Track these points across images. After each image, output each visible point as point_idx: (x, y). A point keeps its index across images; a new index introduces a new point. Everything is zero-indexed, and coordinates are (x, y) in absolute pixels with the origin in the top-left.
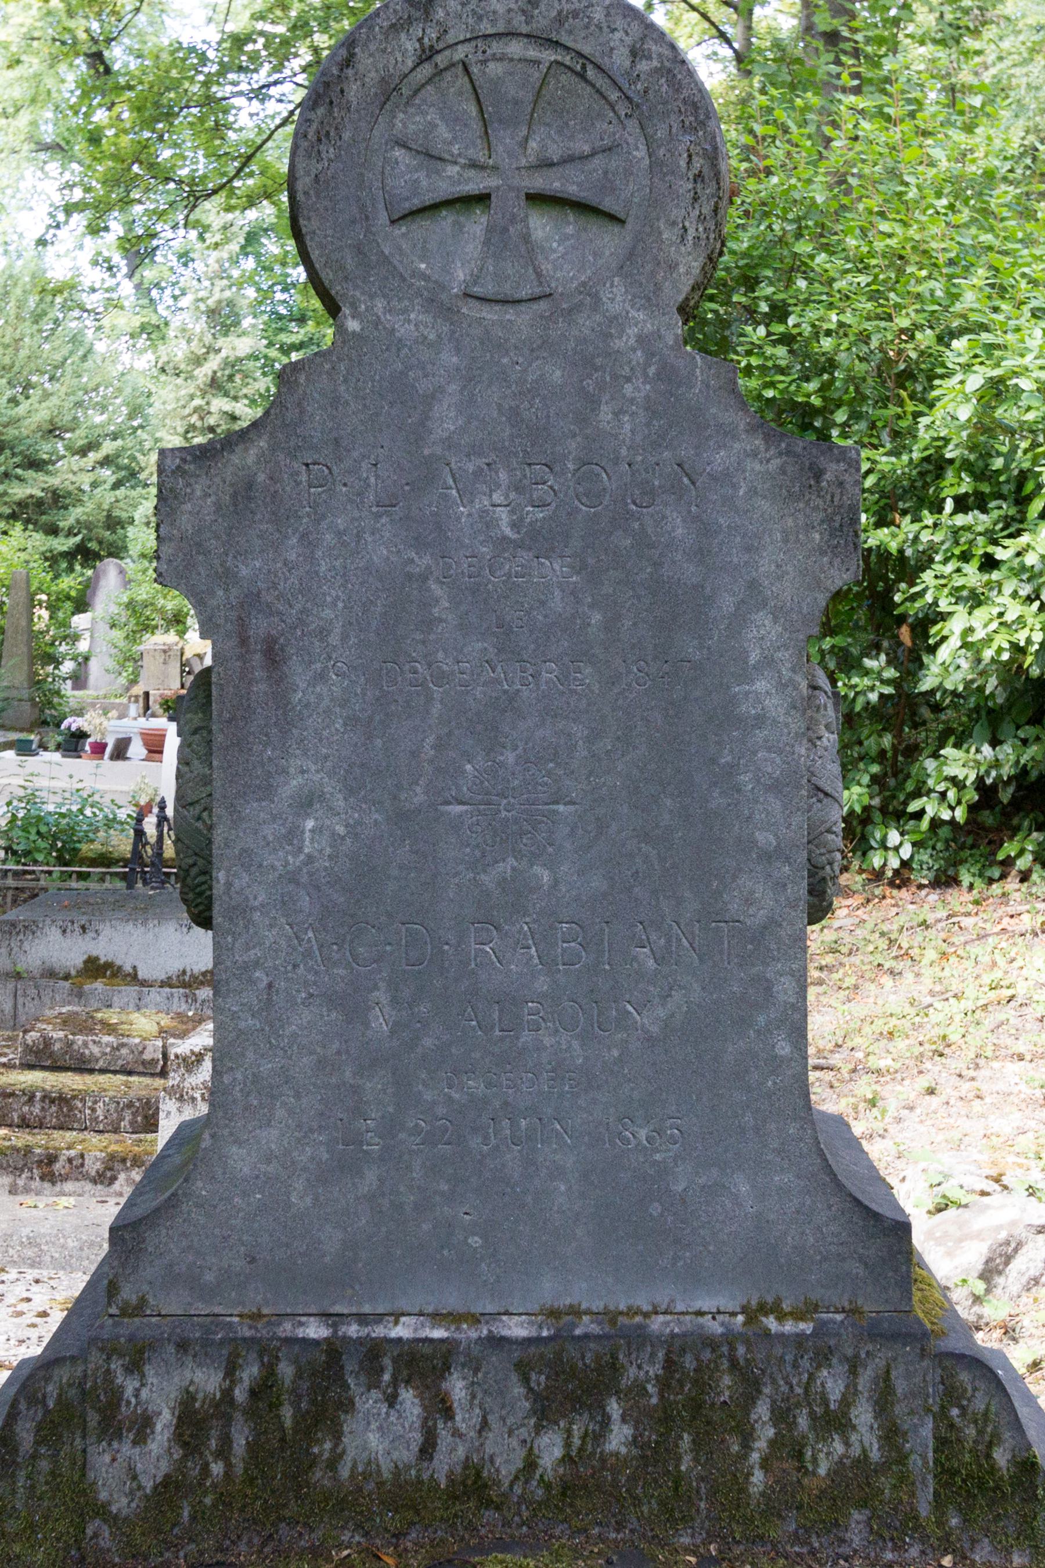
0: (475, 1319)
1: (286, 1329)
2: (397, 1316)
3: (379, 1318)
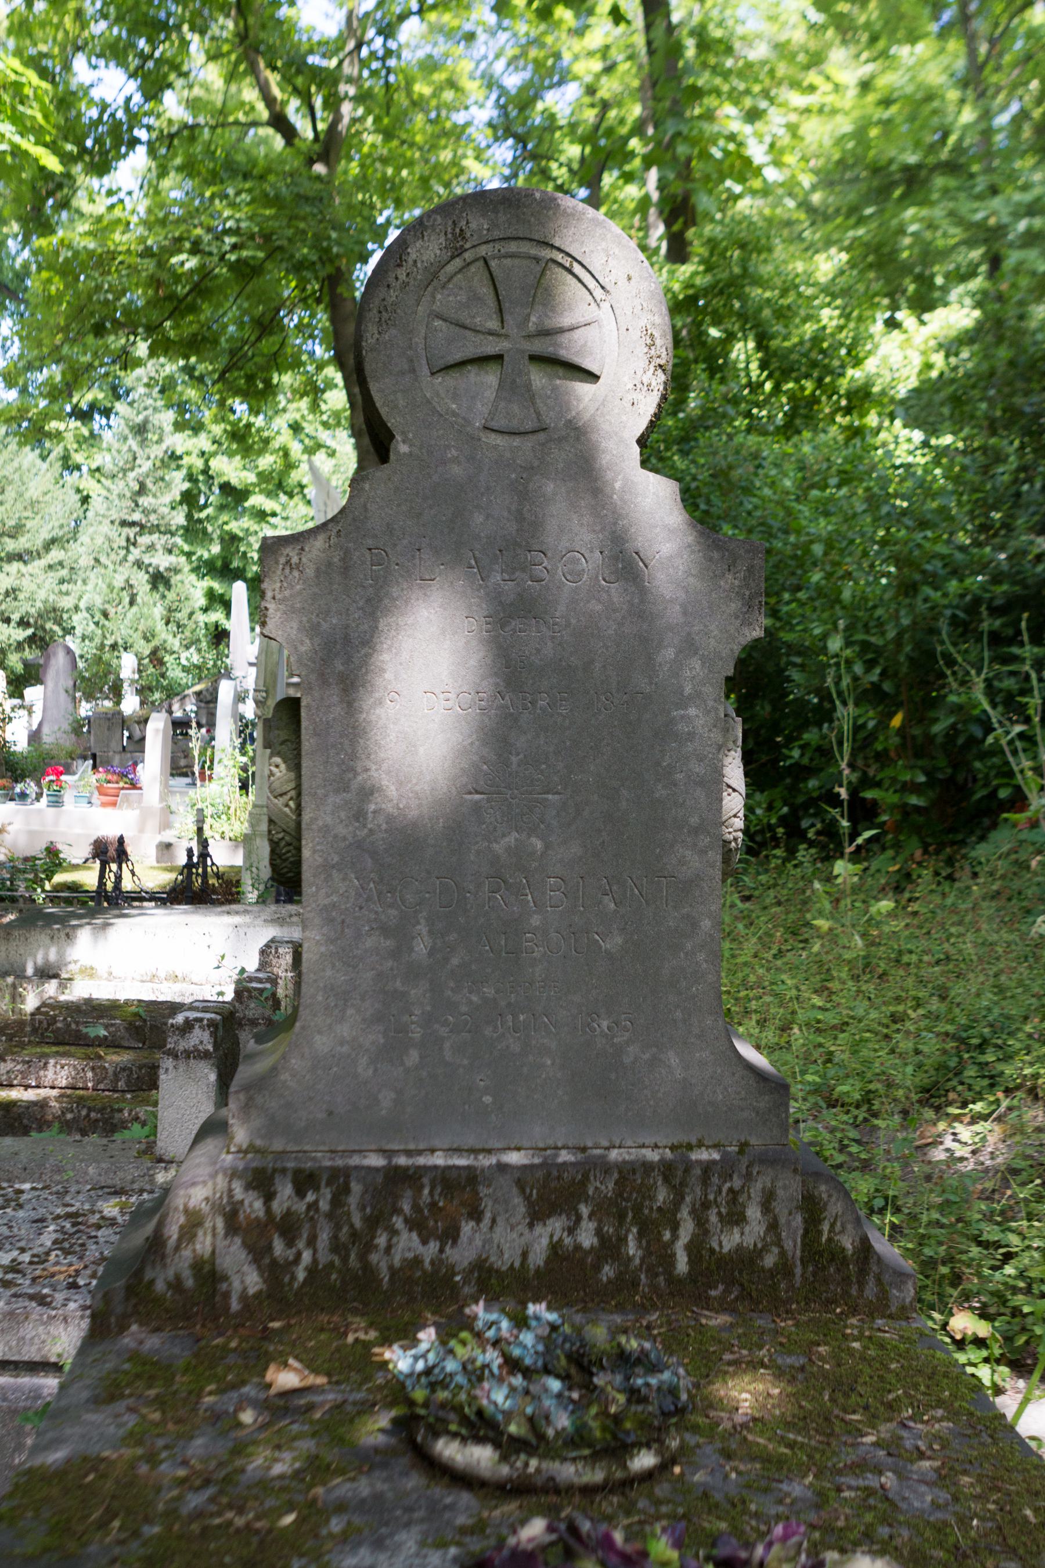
0: (489, 1151)
1: (355, 1161)
2: (433, 1151)
3: (420, 1152)
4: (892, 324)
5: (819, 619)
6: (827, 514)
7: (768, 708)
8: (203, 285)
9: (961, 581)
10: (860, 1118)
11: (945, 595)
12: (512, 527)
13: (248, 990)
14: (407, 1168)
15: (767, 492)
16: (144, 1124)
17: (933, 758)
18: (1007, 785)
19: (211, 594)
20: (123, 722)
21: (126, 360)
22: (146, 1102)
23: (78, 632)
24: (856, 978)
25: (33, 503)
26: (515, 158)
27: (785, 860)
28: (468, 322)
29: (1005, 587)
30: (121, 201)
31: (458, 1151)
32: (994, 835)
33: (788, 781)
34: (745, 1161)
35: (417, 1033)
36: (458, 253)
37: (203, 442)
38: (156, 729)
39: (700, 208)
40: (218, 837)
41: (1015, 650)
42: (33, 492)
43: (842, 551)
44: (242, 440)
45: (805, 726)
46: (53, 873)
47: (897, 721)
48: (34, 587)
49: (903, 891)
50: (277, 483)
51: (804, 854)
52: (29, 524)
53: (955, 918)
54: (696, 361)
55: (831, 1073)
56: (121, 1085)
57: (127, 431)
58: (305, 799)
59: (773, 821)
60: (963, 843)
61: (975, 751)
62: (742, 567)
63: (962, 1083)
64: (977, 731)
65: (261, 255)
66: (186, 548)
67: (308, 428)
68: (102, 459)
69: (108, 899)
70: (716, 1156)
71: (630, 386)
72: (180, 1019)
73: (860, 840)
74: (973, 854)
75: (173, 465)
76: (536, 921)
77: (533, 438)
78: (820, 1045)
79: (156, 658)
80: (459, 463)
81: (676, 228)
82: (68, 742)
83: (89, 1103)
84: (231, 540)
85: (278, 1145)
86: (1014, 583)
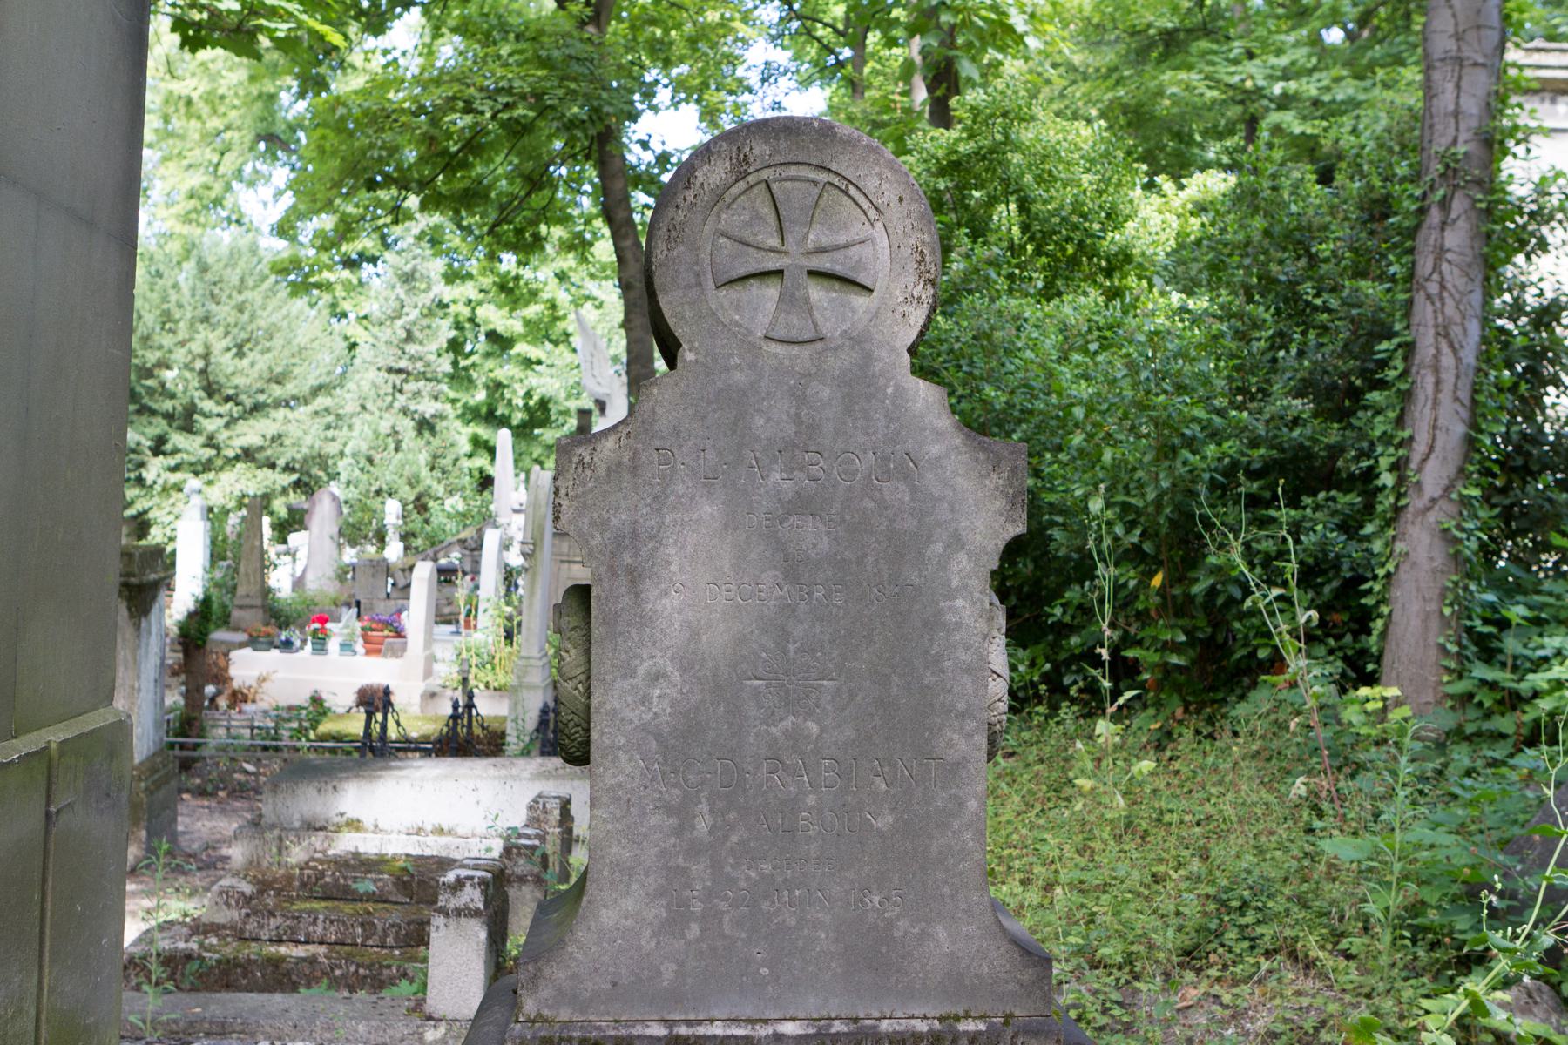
0: (766, 1021)
1: (638, 1030)
2: (712, 1021)
3: (699, 1022)
4: (1150, 186)
5: (1080, 480)
6: (1087, 378)
7: (1031, 566)
8: (474, 145)
9: (1219, 445)
10: (1122, 981)
11: (1204, 458)
12: (791, 430)
13: (518, 847)
14: (688, 1038)
15: (1029, 354)
16: (412, 981)
17: (1193, 617)
18: (1266, 645)
19: (477, 442)
20: (388, 570)
21: (398, 214)
22: (414, 959)
23: (343, 478)
24: (1118, 839)
25: (301, 350)
26: (781, 18)
27: (1048, 717)
28: (750, 239)
29: (1262, 451)
30: (395, 60)
31: (736, 1021)
32: (1253, 695)
33: (1050, 637)
34: (1010, 1032)
35: (697, 908)
36: (742, 176)
37: (469, 290)
38: (423, 572)
39: (963, 74)
40: (482, 687)
41: (1273, 513)
42: (302, 339)
43: (1103, 413)
44: (510, 292)
45: (1067, 583)
46: (318, 722)
47: (1157, 581)
48: (300, 433)
49: (1164, 749)
50: (542, 331)
51: (1066, 711)
52: (296, 371)
53: (1215, 778)
54: (959, 225)
55: (1094, 935)
56: (390, 941)
57: (395, 280)
58: (594, 683)
59: (1036, 679)
60: (1224, 701)
61: (1234, 611)
62: (1006, 468)
63: (1222, 945)
64: (1238, 594)
65: (532, 114)
66: (452, 394)
67: (575, 278)
68: (372, 307)
69: (372, 749)
70: (982, 1027)
71: (901, 299)
72: (451, 877)
73: (1121, 701)
74: (1233, 713)
75: (441, 313)
76: (811, 800)
77: (812, 346)
78: (1083, 906)
79: (421, 505)
80: (742, 370)
81: (939, 93)
82: (332, 589)
83: (358, 960)
84: (496, 387)
85: (564, 1015)
86: (1272, 447)
